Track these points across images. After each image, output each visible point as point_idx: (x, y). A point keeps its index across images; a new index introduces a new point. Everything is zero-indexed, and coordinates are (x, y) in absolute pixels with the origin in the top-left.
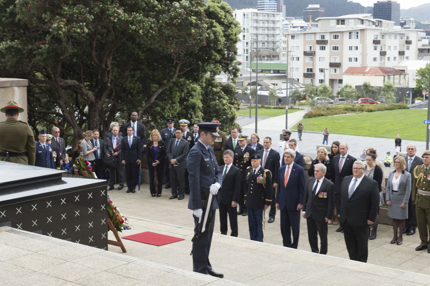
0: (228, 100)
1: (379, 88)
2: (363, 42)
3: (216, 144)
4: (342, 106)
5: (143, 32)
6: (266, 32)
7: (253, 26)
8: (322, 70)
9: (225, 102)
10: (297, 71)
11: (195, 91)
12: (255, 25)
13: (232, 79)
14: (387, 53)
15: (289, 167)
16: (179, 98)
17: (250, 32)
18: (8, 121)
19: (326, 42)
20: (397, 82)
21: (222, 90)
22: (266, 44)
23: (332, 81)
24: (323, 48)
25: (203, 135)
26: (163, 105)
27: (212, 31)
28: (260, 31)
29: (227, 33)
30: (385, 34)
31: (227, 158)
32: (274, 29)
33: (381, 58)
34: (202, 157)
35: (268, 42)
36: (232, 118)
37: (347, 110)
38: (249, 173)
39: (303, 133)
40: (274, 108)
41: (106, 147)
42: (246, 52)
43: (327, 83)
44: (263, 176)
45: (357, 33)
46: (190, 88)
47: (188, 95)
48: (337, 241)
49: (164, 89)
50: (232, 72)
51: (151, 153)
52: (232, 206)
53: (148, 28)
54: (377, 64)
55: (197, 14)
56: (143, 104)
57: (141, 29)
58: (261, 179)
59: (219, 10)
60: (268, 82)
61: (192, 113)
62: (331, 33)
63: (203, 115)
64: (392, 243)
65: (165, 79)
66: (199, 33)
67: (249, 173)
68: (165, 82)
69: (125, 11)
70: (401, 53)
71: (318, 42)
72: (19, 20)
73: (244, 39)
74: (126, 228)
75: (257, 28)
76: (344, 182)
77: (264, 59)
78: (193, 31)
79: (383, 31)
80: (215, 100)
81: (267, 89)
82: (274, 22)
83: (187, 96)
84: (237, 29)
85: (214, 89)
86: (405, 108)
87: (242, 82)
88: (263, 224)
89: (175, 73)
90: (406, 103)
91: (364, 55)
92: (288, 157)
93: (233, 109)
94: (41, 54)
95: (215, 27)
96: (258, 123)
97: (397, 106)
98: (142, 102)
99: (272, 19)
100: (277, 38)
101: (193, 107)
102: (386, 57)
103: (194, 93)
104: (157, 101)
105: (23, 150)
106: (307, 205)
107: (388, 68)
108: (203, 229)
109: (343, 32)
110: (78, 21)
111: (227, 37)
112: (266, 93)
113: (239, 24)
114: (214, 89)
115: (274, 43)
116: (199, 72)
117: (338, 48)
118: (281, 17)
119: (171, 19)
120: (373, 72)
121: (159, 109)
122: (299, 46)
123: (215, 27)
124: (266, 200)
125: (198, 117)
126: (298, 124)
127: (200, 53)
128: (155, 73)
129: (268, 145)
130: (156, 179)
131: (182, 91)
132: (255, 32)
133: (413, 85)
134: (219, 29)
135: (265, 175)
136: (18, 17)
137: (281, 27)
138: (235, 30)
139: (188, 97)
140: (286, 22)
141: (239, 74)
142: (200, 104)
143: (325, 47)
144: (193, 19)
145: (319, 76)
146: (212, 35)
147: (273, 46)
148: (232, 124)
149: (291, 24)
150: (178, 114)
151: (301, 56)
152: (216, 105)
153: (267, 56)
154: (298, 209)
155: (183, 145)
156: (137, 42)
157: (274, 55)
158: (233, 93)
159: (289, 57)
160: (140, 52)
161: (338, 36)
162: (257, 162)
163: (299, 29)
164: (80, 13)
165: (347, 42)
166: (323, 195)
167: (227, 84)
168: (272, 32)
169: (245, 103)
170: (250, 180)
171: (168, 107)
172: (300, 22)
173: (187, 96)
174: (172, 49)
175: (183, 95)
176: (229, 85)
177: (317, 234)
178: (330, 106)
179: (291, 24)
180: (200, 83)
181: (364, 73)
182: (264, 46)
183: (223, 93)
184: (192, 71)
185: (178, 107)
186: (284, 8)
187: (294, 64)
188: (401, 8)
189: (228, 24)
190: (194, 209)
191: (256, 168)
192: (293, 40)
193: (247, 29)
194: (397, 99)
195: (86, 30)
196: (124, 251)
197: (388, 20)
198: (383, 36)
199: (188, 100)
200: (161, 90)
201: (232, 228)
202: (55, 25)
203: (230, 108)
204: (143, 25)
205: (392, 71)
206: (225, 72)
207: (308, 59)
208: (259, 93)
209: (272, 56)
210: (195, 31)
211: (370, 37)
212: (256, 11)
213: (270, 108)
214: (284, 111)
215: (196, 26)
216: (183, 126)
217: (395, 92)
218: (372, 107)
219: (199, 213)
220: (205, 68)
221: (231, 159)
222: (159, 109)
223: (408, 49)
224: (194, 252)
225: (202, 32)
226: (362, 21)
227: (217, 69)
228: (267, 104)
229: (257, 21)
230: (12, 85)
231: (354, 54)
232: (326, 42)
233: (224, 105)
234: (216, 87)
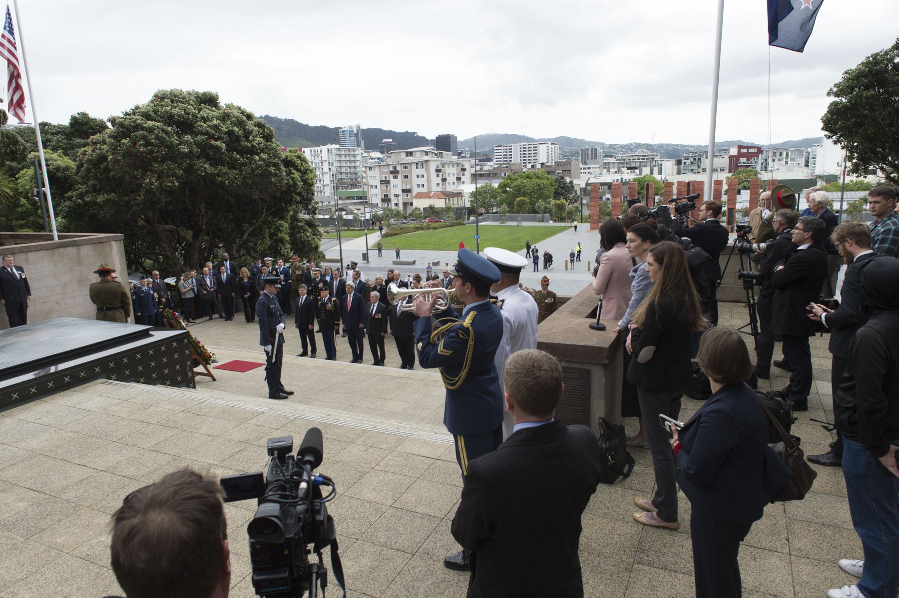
2: (427, 171)
4: (413, 226)
6: (348, 164)
8: (396, 196)
10: (375, 196)
12: (338, 159)
18: (101, 282)
19: (398, 172)
20: (455, 203)
23: (405, 204)
24: (396, 177)
28: (344, 164)
37: (417, 229)
41: (201, 284)
43: (401, 207)
51: (242, 288)
54: (440, 189)
55: (276, 165)
59: (295, 159)
60: (352, 207)
69: (211, 165)
70: (459, 179)
71: (391, 172)
72: (114, 176)
74: (214, 361)
75: (340, 161)
81: (352, 213)
82: (354, 156)
86: (462, 224)
91: (429, 181)
94: (138, 205)
99: (352, 153)
100: (358, 170)
101: (282, 240)
105: (119, 305)
108: (274, 360)
110: (168, 176)
111: (305, 181)
112: (350, 217)
115: (356, 173)
118: (359, 151)
119: (253, 170)
120: (437, 196)
130: (249, 308)
132: (339, 165)
133: (468, 205)
134: (297, 175)
136: (112, 173)
140: (365, 155)
144: (272, 169)
145: (394, 200)
151: (379, 185)
164: (169, 169)
165: (415, 172)
168: (353, 164)
172: (377, 155)
174: (256, 195)
178: (403, 226)
181: (430, 197)
186: (363, 142)
187: (373, 191)
188: (458, 140)
195: (177, 184)
196: (214, 380)
197: (175, 384)
198: (443, 166)
202: (147, 181)
211: (433, 167)
212: (338, 146)
215: (275, 175)
218: (436, 225)
219: (269, 348)
221: (305, 291)
223: (463, 175)
224: (268, 378)
226: (427, 153)
229: (340, 155)
230: (109, 240)
231: (421, 181)
232: (398, 172)
234: (300, 221)
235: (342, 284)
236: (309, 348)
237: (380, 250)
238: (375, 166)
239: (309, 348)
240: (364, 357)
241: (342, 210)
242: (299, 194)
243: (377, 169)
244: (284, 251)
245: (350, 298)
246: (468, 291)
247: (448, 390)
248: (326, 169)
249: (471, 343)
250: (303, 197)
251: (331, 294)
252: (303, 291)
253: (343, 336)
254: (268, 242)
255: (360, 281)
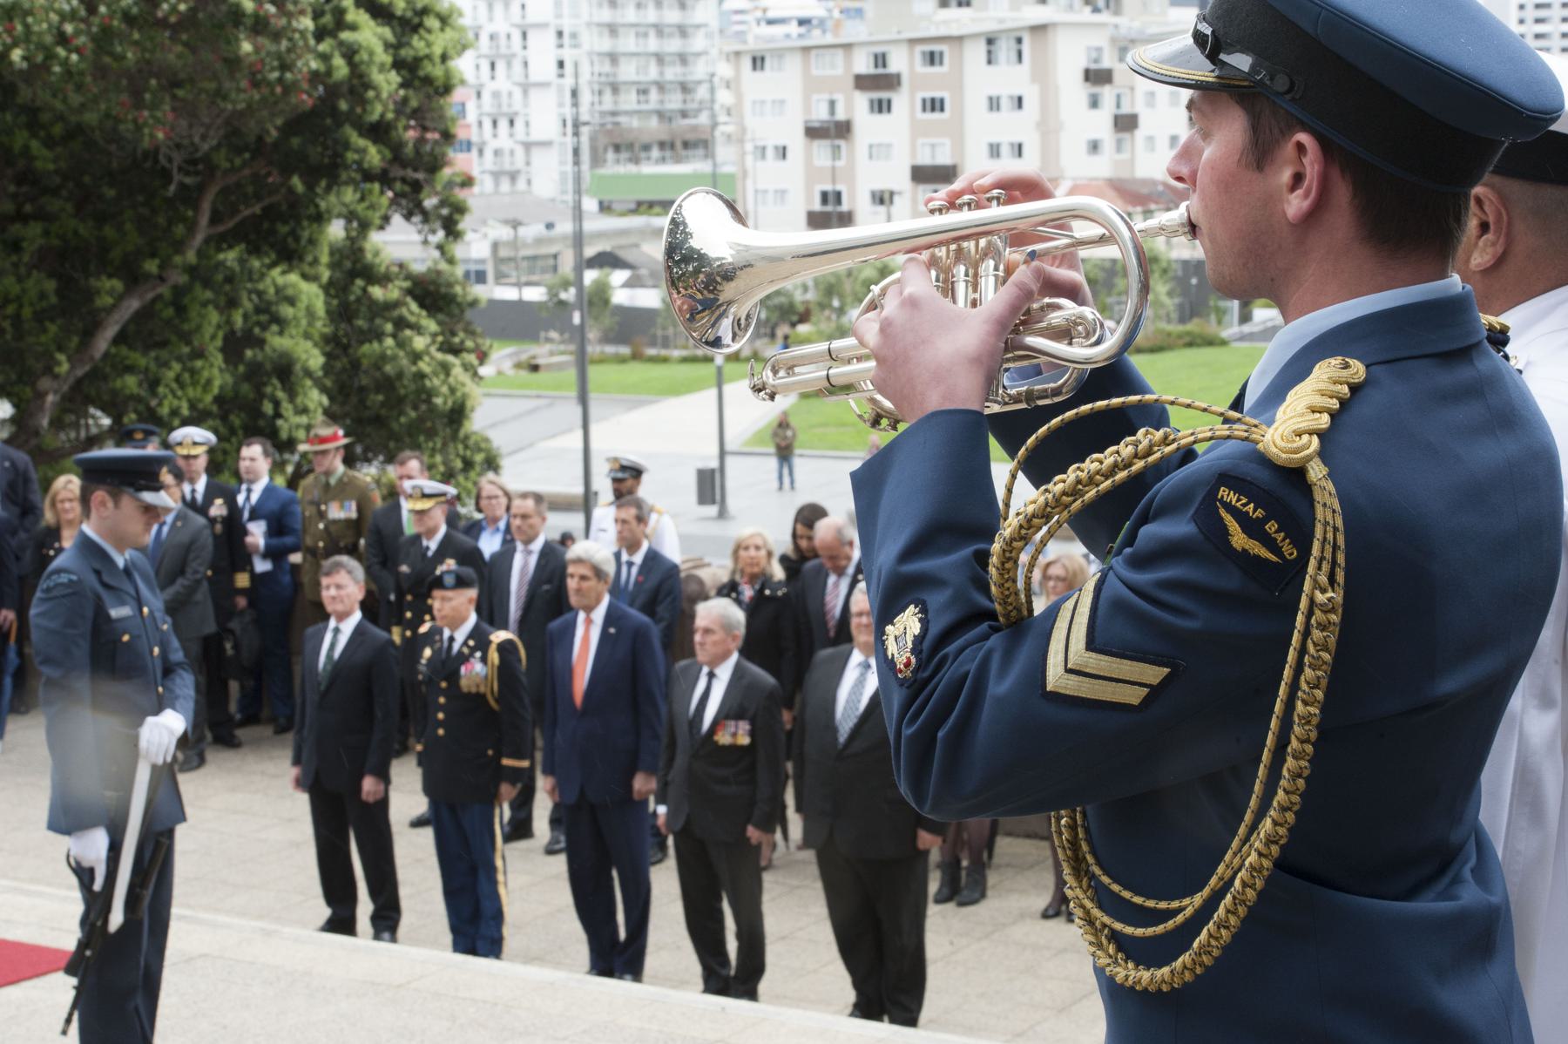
0: (434, 335)
1: (1108, 265)
2: (1043, 76)
3: (332, 529)
5: (24, 58)
6: (653, 44)
7: (596, 19)
9: (419, 343)
11: (292, 301)
12: (606, 15)
13: (440, 247)
14: (1142, 121)
15: (589, 621)
16: (221, 334)
17: (586, 47)
21: (409, 292)
22: (654, 95)
24: (882, 107)
25: (103, 504)
26: (153, 366)
27: (341, 44)
28: (628, 43)
29: (405, 53)
30: (1133, 41)
31: (339, 587)
32: (683, 31)
33: (1119, 143)
34: (99, 598)
35: (661, 87)
36: (453, 411)
38: (428, 652)
39: (797, 462)
40: (685, 360)
42: (569, 129)
44: (484, 660)
45: (1019, 41)
46: (272, 291)
47: (264, 318)
48: (798, 920)
49: (150, 296)
50: (440, 217)
52: (364, 796)
53: (48, 39)
54: (1103, 167)
56: (59, 364)
57: (15, 45)
58: (476, 672)
61: (280, 394)
62: (913, 42)
63: (325, 401)
64: (1046, 915)
65: (153, 255)
66: (279, 56)
67: (428, 652)
68: (151, 266)
71: (862, 82)
73: (561, 76)
75: (613, 29)
76: (815, 676)
77: (649, 158)
78: (247, 47)
79: (1123, 32)
80: (379, 336)
83: (258, 323)
84: (449, 34)
85: (377, 292)
87: (555, 256)
88: (499, 863)
89: (192, 227)
90: (1219, 322)
91: (1048, 128)
92: (583, 578)
93: (457, 371)
95: (353, 27)
96: (594, 429)
97: (1180, 336)
98: (52, 358)
100: (699, 70)
101: (285, 370)
102: (1140, 134)
103: (287, 311)
104: (124, 350)
106: (670, 778)
107: (1144, 182)
108: (116, 919)
109: (960, 39)
111: (409, 68)
113: (460, 15)
114: (377, 292)
115: (685, 88)
116: (299, 222)
117: (942, 101)
121: (131, 382)
122: (782, 102)
123: (353, 27)
124: (506, 762)
125: (304, 411)
126: (775, 424)
127: (295, 142)
128: (109, 231)
129: (531, 526)
131: (233, 303)
132: (606, 44)
134: (369, 35)
135: (494, 656)
137: (714, 24)
138: (439, 41)
139: (264, 328)
141: (464, 224)
142: (315, 359)
143: (889, 102)
146: (339, 62)
147: (685, 101)
148: (454, 437)
149: (756, 8)
150: (219, 400)
152: (383, 358)
153: (662, 145)
154: (636, 796)
155: (184, 537)
156: (19, 100)
157: (690, 137)
158: (459, 305)
159: (749, 147)
160: (35, 145)
161: (941, 54)
162: (454, 603)
163: (793, 29)
165: (979, 78)
166: (734, 735)
167: (429, 270)
169: (563, 342)
170: (430, 682)
171: (171, 374)
173: (258, 323)
174: (158, 129)
175: (238, 321)
176: (438, 273)
177: (720, 900)
179: (756, 8)
180: (307, 269)
182: (647, 102)
183: (414, 306)
184: (271, 213)
185: (216, 372)
189: (409, 14)
190: (67, 831)
191: (455, 623)
192: (758, 74)
193: (574, 36)
194: (1181, 307)
199: (261, 343)
200: (134, 304)
201: (374, 894)
203: (446, 368)
204: (27, 26)
205: (1160, 194)
206: (408, 216)
207: (822, 149)
208: (620, 297)
209: (679, 144)
210: (257, 50)
213: (665, 360)
214: (707, 371)
216: (187, 457)
217: (1175, 278)
219: (94, 846)
220: (317, 206)
222: (131, 382)
225: (289, 50)
227: (372, 207)
228: (653, 344)
231: (1009, 127)
233: (416, 357)
234: (384, 280)
235: (552, 565)
236: (365, 907)
237: (785, 453)
238: (780, 53)
239: (365, 907)
240: (651, 962)
241: (609, 260)
242: (379, 132)
243: (793, 64)
244: (290, 422)
245: (587, 637)
246: (1296, 205)
247: (1116, 995)
248: (542, 68)
249: (1320, 592)
250: (396, 149)
251: (491, 612)
252: (345, 586)
253: (550, 851)
254: (217, 374)
255: (653, 557)
